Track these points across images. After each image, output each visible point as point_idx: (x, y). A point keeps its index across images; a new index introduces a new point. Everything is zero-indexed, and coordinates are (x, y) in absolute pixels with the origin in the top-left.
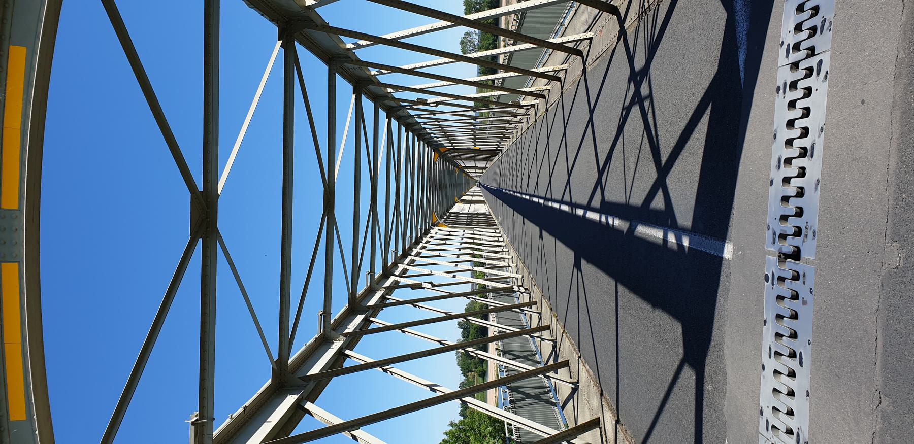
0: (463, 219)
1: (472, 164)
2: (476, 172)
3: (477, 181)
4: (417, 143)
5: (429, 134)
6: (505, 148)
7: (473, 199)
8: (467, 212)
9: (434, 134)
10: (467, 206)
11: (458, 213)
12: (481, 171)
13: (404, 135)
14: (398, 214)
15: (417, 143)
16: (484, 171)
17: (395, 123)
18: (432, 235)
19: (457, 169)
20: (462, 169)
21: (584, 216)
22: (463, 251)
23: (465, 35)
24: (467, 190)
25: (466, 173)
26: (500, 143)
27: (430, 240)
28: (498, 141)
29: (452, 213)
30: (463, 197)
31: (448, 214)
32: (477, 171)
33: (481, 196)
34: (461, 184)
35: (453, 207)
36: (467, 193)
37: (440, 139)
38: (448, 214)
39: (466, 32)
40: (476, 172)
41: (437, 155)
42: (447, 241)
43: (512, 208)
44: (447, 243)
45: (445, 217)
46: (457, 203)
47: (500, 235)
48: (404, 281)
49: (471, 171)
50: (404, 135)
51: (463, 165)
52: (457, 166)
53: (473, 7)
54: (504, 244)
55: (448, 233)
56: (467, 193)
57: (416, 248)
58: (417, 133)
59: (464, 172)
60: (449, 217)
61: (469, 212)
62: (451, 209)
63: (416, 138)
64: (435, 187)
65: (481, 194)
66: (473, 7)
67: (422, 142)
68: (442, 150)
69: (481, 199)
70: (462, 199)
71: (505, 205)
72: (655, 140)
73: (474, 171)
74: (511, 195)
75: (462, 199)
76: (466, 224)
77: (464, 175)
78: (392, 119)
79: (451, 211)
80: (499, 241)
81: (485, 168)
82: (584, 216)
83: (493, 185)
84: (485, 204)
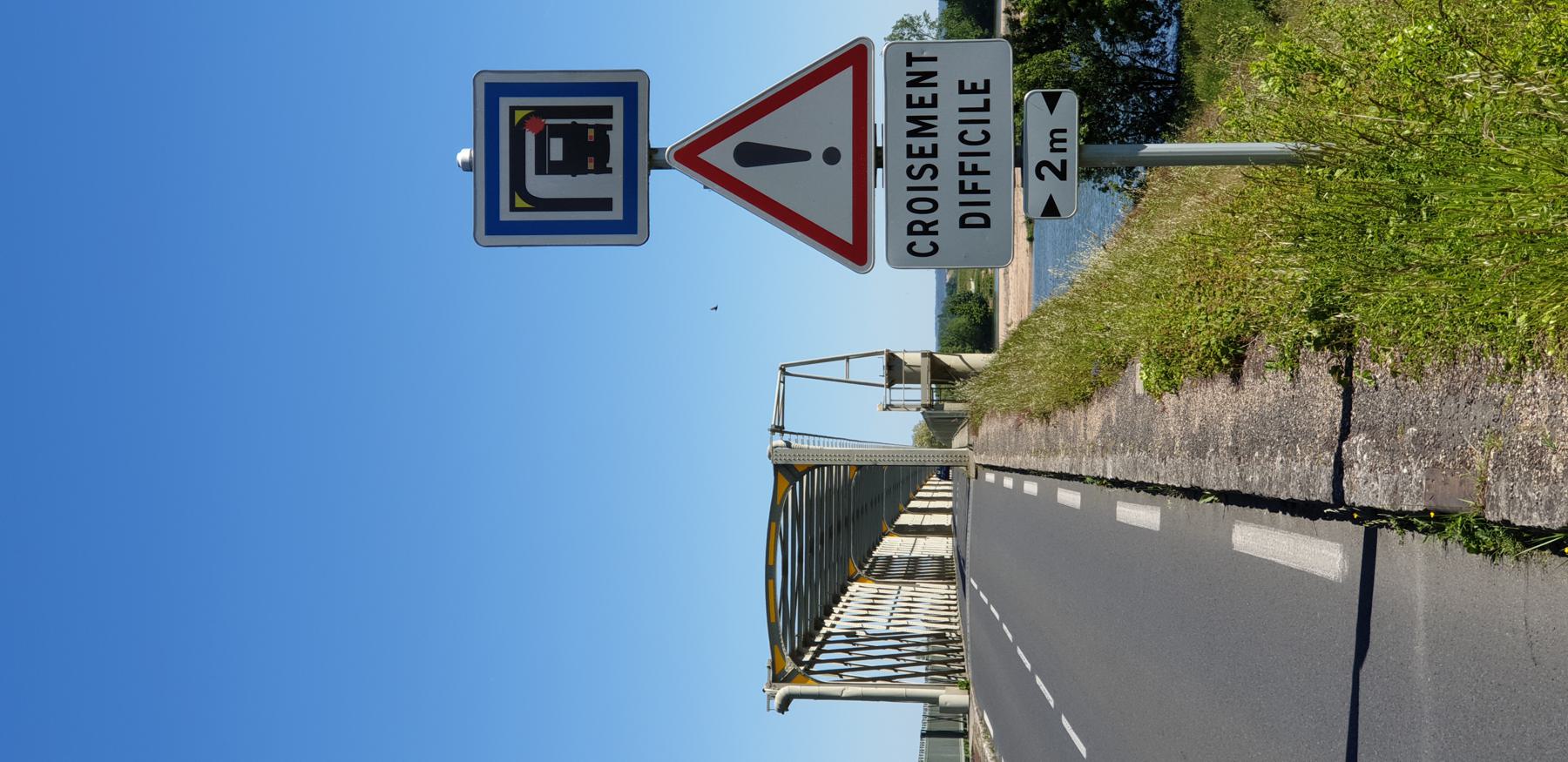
0: (899, 569)
7: (926, 523)
8: (908, 555)
10: (909, 540)
11: (890, 559)
18: (852, 594)
22: (893, 622)
23: (896, 28)
24: (918, 487)
29: (876, 558)
30: (912, 502)
31: (871, 560)
35: (879, 545)
38: (871, 560)
39: (899, 18)
42: (909, 621)
44: (925, 638)
45: (867, 566)
46: (856, 580)
48: (833, 630)
55: (871, 601)
56: (913, 504)
57: (829, 619)
60: (873, 566)
61: (913, 555)
62: (875, 549)
70: (909, 506)
72: (781, 633)
75: (909, 506)
76: (904, 578)
79: (875, 554)
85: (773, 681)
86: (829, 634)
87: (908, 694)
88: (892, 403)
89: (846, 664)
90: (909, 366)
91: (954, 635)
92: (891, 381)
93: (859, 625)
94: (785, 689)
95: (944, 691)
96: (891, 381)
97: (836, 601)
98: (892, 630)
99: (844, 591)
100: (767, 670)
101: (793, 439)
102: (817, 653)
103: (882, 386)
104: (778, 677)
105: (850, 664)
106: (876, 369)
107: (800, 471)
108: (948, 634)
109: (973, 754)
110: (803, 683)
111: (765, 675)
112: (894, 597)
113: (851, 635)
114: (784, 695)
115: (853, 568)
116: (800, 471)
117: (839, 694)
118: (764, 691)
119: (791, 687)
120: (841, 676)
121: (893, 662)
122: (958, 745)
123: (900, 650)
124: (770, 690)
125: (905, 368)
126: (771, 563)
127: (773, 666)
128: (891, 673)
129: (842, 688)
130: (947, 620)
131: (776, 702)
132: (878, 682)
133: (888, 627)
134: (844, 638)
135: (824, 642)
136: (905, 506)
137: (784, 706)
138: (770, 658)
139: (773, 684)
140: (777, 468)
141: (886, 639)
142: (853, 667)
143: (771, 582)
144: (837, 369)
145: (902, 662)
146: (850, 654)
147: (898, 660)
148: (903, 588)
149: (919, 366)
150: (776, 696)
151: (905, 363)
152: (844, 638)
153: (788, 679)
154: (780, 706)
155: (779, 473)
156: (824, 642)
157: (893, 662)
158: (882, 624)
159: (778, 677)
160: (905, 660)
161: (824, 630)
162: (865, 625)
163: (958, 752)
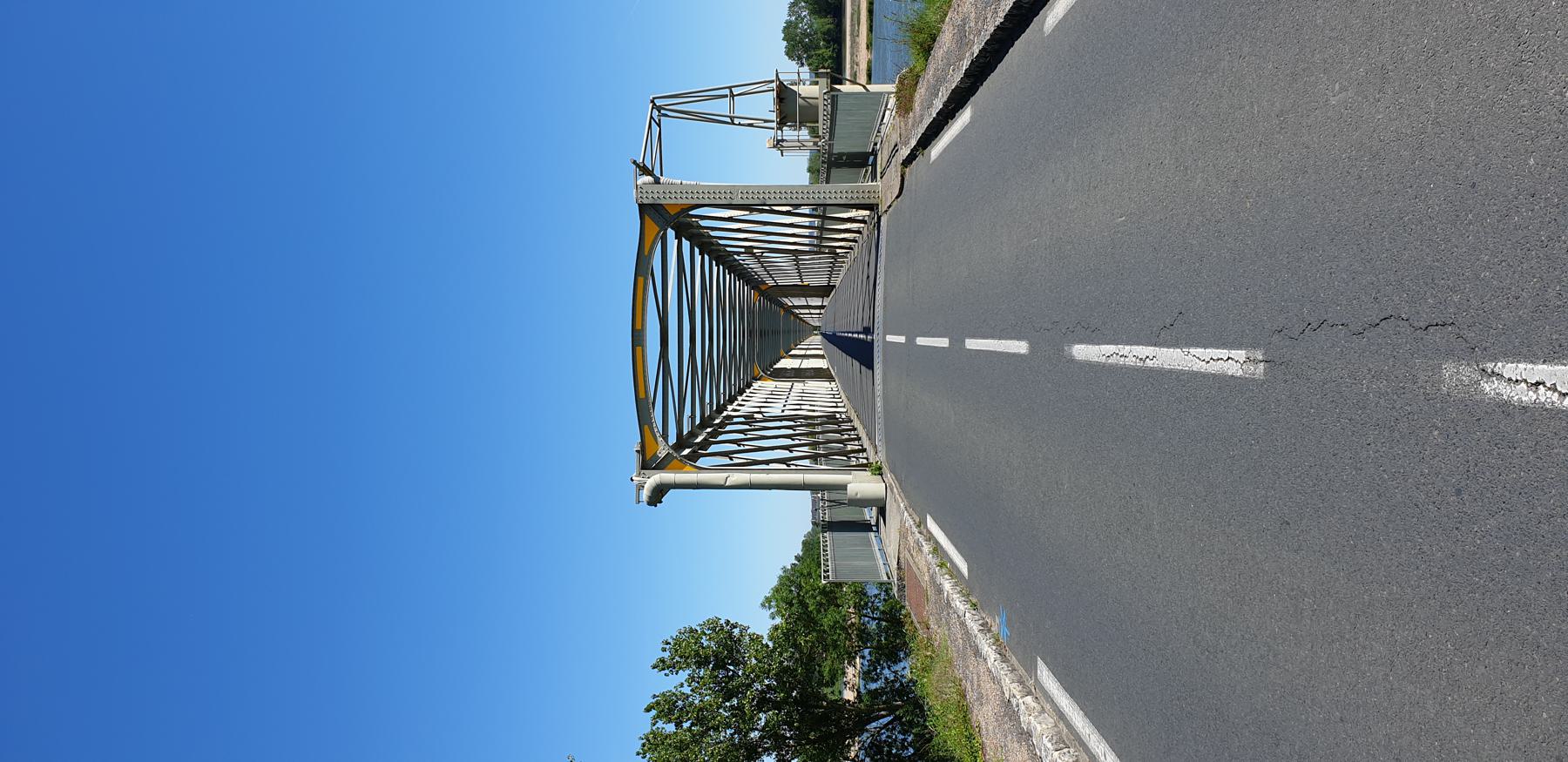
1: (802, 302)
2: (811, 314)
3: (816, 328)
4: (715, 269)
5: (742, 265)
6: (837, 281)
9: (743, 260)
12: (818, 311)
13: (698, 258)
14: (694, 369)
15: (715, 269)
16: (822, 311)
17: (686, 244)
19: (782, 310)
20: (789, 310)
21: (867, 336)
25: (796, 316)
26: (832, 269)
27: (738, 408)
28: (830, 267)
32: (812, 311)
33: (822, 357)
34: (789, 332)
36: (793, 352)
37: (746, 262)
40: (811, 314)
41: (757, 294)
43: (859, 361)
46: (759, 380)
47: (840, 400)
49: (802, 311)
50: (698, 258)
51: (790, 304)
52: (782, 305)
53: (800, 42)
54: (845, 410)
55: (765, 400)
56: (799, 347)
58: (715, 255)
59: (793, 313)
63: (697, 250)
64: (751, 333)
65: (820, 347)
66: (800, 42)
67: (706, 257)
68: (763, 287)
69: (822, 364)
71: (849, 358)
73: (807, 311)
74: (850, 337)
77: (792, 317)
78: (683, 239)
80: (837, 407)
81: (822, 307)
82: (867, 336)
83: (829, 331)
84: (830, 378)
85: (642, 469)
86: (729, 417)
87: (806, 481)
88: (784, 138)
89: (739, 445)
90: (803, 98)
91: (843, 416)
92: (781, 123)
93: (758, 410)
94: (656, 478)
95: (851, 477)
96: (781, 123)
97: (741, 392)
98: (786, 413)
99: (749, 386)
100: (636, 453)
101: (765, 414)
102: (711, 435)
103: (773, 129)
104: (648, 463)
105: (743, 445)
106: (766, 106)
107: (672, 213)
108: (838, 416)
109: (899, 568)
110: (679, 469)
111: (635, 460)
112: (785, 397)
113: (749, 419)
114: (654, 485)
115: (758, 371)
116: (672, 213)
117: (723, 483)
118: (632, 480)
119: (663, 475)
120: (731, 459)
121: (788, 442)
122: (869, 544)
123: (795, 430)
124: (638, 479)
125: (799, 101)
126: (638, 327)
127: (642, 451)
128: (785, 454)
129: (726, 475)
130: (834, 405)
131: (645, 494)
132: (773, 466)
133: (783, 411)
134: (742, 420)
135: (722, 425)
136: (787, 353)
137: (658, 494)
138: (640, 441)
139: (643, 471)
140: (642, 207)
141: (781, 421)
142: (747, 447)
143: (639, 349)
144: (721, 107)
145: (797, 442)
146: (746, 435)
147: (793, 440)
148: (795, 384)
149: (817, 98)
150: (646, 486)
151: (800, 95)
152: (742, 420)
153: (661, 465)
154: (650, 498)
155: (647, 217)
156: (722, 425)
157: (788, 442)
158: (778, 408)
159: (648, 463)
160: (800, 440)
161: (725, 414)
162: (763, 410)
163: (873, 558)
